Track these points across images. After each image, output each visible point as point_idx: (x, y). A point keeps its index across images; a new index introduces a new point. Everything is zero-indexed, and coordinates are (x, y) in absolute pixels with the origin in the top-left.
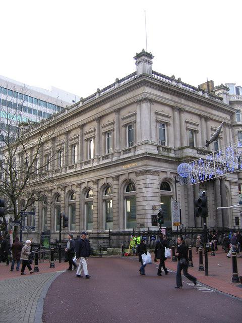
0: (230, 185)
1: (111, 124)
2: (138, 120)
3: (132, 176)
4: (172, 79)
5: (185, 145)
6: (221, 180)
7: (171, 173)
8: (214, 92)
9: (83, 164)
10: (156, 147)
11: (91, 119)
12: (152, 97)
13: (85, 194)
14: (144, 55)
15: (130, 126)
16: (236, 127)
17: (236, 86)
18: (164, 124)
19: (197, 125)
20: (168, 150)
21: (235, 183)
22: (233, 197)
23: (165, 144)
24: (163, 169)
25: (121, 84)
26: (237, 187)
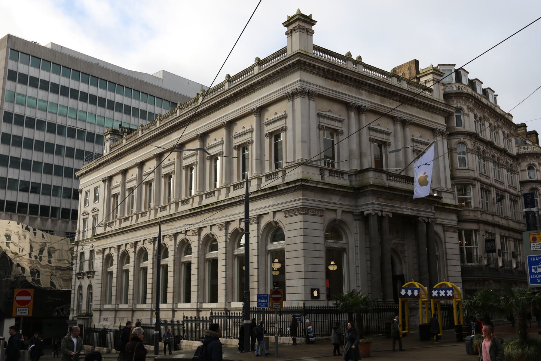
0: (444, 231)
1: (280, 119)
3: (279, 217)
4: (347, 58)
5: (366, 166)
6: (428, 224)
7: (343, 211)
8: (419, 79)
9: (264, 179)
10: (319, 170)
12: (313, 88)
14: (298, 19)
15: (276, 135)
16: (455, 137)
17: (456, 67)
18: (335, 132)
19: (388, 134)
20: (341, 174)
21: (451, 228)
22: (449, 251)
23: (333, 166)
24: (330, 206)
25: (265, 66)
26: (456, 235)
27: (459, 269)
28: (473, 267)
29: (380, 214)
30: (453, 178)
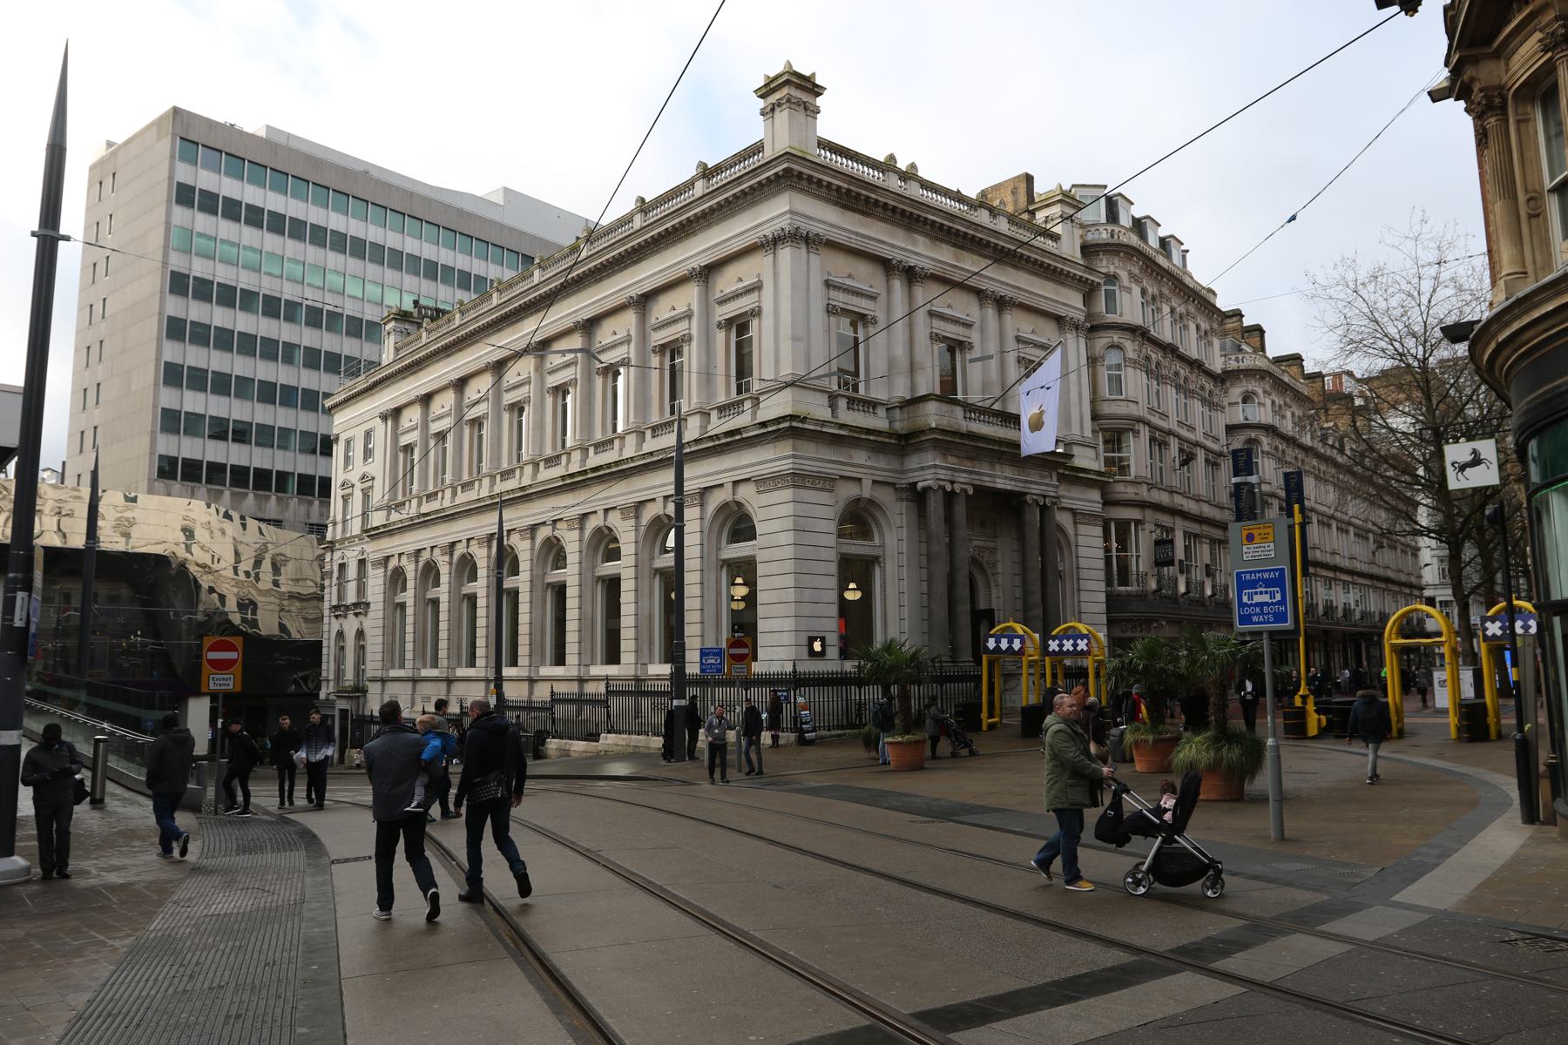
0: (1075, 523)
2: (767, 307)
3: (746, 494)
4: (888, 166)
5: (922, 392)
7: (874, 482)
8: (1032, 213)
11: (683, 270)
12: (816, 228)
13: (654, 542)
14: (787, 82)
15: (740, 325)
16: (1102, 334)
19: (969, 325)
20: (871, 405)
23: (856, 389)
25: (717, 181)
26: (1098, 531)
27: (1102, 597)
28: (1129, 595)
29: (949, 488)
30: (1095, 417)
